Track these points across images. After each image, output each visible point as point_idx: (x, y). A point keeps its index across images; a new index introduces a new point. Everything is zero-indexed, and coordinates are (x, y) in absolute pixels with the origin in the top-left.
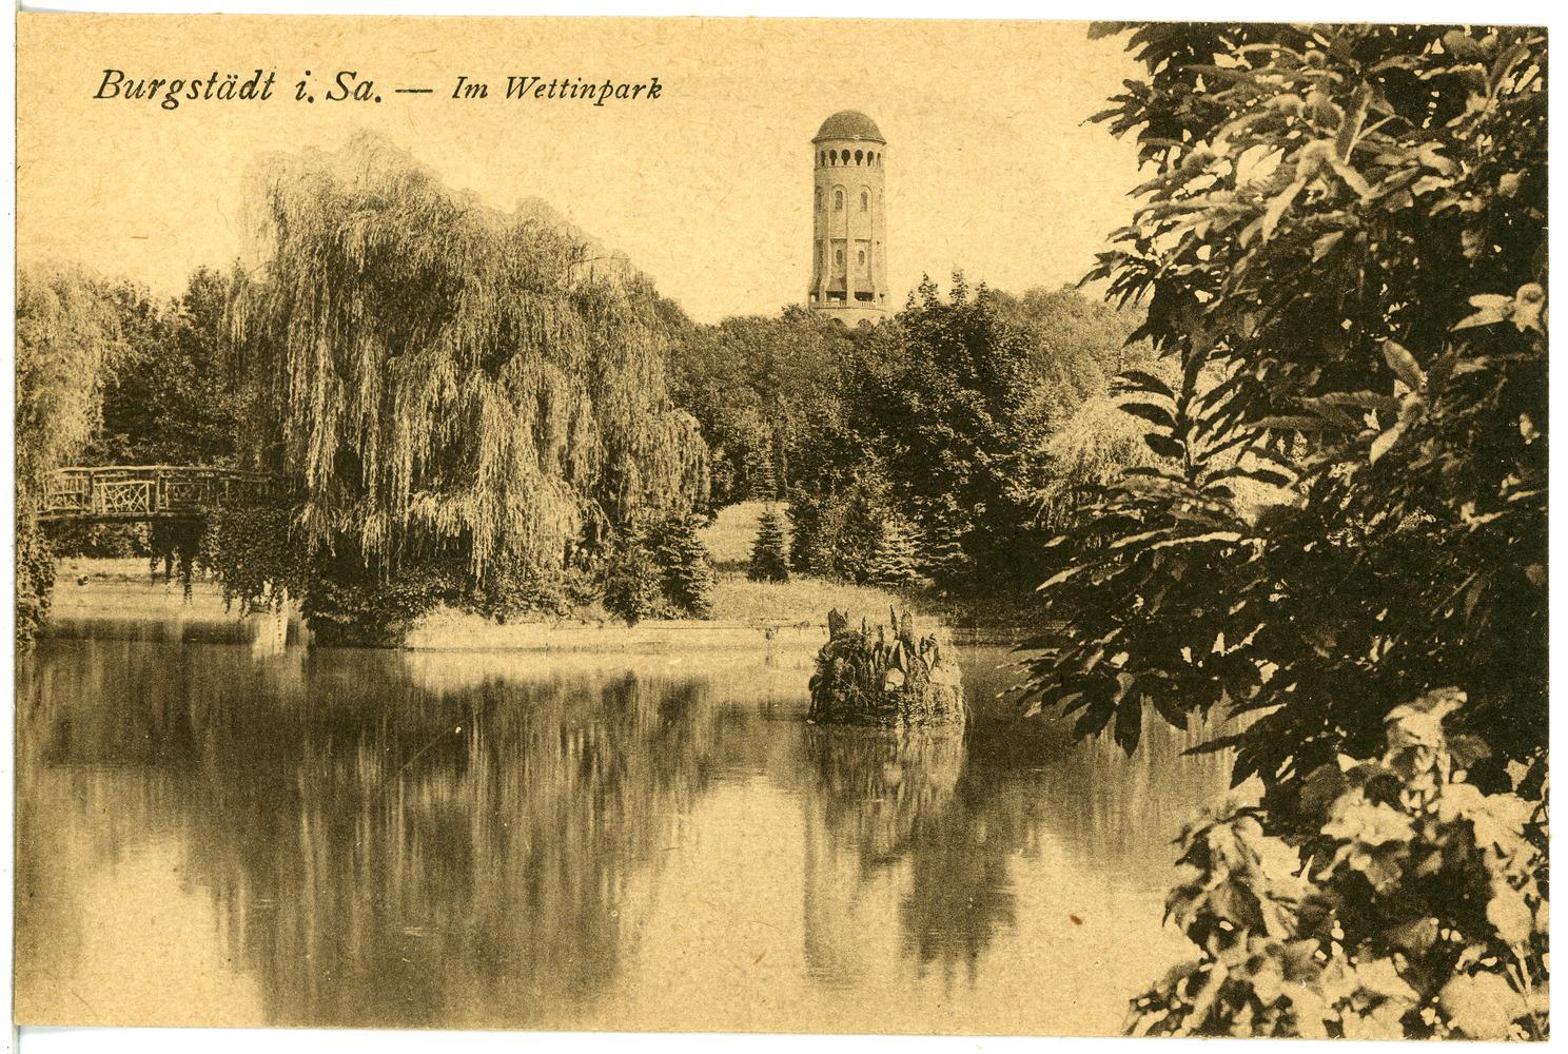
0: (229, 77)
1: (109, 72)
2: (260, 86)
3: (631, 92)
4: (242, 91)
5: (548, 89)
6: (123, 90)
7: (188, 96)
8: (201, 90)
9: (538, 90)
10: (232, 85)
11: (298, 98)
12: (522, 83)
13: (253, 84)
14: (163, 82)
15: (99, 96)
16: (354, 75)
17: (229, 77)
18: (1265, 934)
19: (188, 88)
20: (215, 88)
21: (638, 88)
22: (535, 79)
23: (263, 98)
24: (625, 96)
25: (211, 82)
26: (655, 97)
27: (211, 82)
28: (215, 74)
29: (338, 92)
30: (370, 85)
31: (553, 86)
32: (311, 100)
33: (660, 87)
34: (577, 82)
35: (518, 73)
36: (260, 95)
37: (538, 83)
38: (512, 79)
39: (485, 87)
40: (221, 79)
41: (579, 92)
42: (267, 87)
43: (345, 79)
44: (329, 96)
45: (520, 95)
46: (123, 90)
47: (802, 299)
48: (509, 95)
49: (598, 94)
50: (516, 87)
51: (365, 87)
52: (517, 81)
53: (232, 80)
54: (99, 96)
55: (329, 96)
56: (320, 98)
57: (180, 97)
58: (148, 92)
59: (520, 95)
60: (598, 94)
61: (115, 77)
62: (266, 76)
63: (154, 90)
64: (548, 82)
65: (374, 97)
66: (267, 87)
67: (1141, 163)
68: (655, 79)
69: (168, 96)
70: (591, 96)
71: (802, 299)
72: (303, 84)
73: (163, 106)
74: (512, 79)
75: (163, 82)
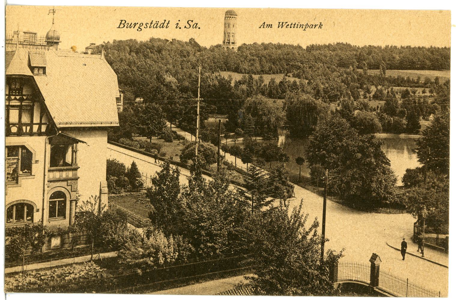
0: (156, 22)
1: (122, 21)
2: (165, 25)
3: (313, 27)
4: (160, 26)
5: (290, 25)
6: (126, 26)
7: (145, 27)
8: (148, 26)
9: (287, 26)
10: (157, 24)
11: (176, 28)
12: (282, 24)
13: (164, 24)
14: (137, 23)
15: (119, 27)
16: (192, 21)
17: (156, 22)
18: (92, 54)
19: (144, 25)
20: (152, 25)
21: (316, 26)
22: (286, 23)
23: (166, 28)
24: (162, 27)
25: (151, 23)
26: (321, 28)
27: (151, 23)
28: (152, 21)
29: (188, 26)
30: (197, 24)
31: (291, 25)
32: (180, 28)
33: (322, 25)
34: (298, 24)
35: (281, 21)
36: (165, 27)
37: (287, 24)
38: (279, 23)
39: (272, 25)
40: (154, 22)
41: (299, 26)
42: (167, 25)
43: (190, 22)
44: (185, 27)
45: (282, 27)
46: (126, 26)
47: (221, 43)
48: (279, 27)
49: (304, 27)
50: (281, 25)
51: (195, 25)
52: (281, 24)
53: (157, 23)
54: (119, 27)
55: (185, 27)
57: (142, 28)
58: (133, 26)
59: (282, 27)
60: (304, 27)
61: (123, 22)
62: (167, 22)
63: (135, 26)
64: (294, 23)
65: (198, 27)
66: (167, 25)
67: (97, 50)
68: (321, 23)
69: (139, 27)
70: (302, 28)
71: (221, 43)
72: (178, 24)
73: (138, 30)
74: (279, 23)
75: (137, 23)
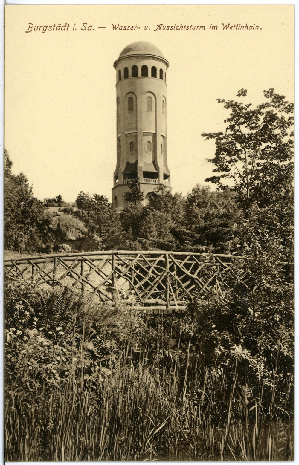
2: (67, 27)
25: (55, 26)
27: (55, 26)
56: (79, 30)
